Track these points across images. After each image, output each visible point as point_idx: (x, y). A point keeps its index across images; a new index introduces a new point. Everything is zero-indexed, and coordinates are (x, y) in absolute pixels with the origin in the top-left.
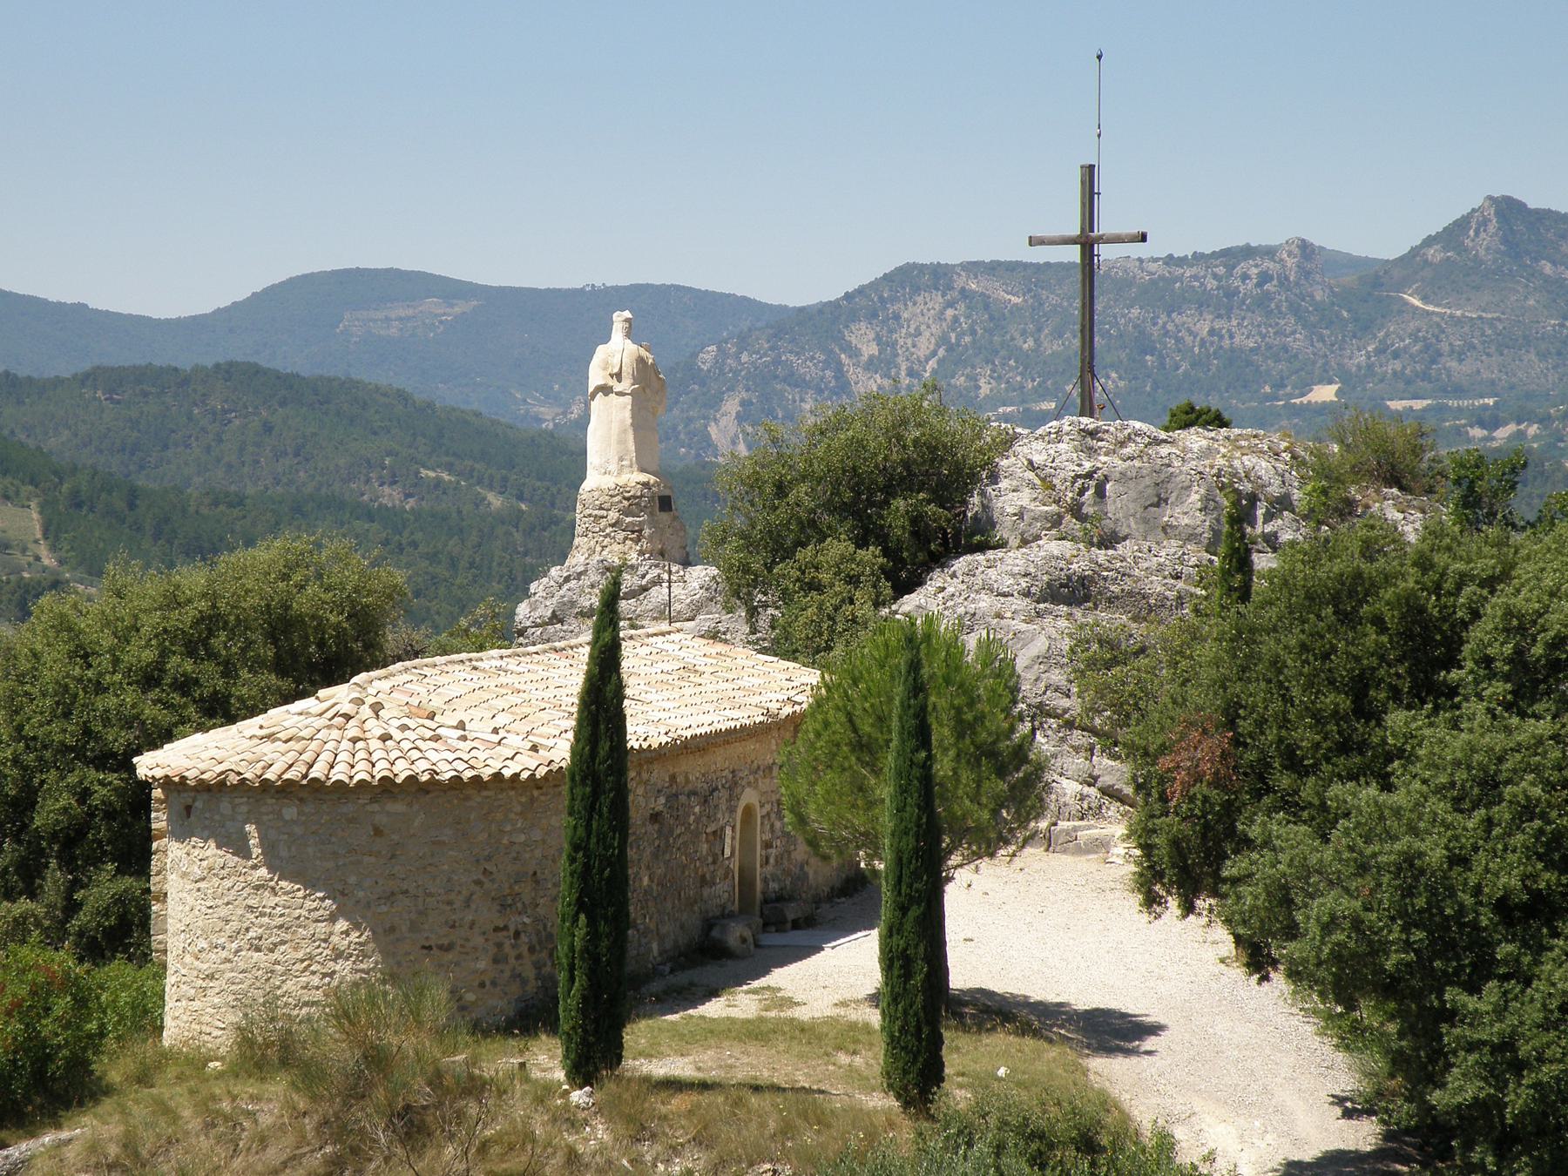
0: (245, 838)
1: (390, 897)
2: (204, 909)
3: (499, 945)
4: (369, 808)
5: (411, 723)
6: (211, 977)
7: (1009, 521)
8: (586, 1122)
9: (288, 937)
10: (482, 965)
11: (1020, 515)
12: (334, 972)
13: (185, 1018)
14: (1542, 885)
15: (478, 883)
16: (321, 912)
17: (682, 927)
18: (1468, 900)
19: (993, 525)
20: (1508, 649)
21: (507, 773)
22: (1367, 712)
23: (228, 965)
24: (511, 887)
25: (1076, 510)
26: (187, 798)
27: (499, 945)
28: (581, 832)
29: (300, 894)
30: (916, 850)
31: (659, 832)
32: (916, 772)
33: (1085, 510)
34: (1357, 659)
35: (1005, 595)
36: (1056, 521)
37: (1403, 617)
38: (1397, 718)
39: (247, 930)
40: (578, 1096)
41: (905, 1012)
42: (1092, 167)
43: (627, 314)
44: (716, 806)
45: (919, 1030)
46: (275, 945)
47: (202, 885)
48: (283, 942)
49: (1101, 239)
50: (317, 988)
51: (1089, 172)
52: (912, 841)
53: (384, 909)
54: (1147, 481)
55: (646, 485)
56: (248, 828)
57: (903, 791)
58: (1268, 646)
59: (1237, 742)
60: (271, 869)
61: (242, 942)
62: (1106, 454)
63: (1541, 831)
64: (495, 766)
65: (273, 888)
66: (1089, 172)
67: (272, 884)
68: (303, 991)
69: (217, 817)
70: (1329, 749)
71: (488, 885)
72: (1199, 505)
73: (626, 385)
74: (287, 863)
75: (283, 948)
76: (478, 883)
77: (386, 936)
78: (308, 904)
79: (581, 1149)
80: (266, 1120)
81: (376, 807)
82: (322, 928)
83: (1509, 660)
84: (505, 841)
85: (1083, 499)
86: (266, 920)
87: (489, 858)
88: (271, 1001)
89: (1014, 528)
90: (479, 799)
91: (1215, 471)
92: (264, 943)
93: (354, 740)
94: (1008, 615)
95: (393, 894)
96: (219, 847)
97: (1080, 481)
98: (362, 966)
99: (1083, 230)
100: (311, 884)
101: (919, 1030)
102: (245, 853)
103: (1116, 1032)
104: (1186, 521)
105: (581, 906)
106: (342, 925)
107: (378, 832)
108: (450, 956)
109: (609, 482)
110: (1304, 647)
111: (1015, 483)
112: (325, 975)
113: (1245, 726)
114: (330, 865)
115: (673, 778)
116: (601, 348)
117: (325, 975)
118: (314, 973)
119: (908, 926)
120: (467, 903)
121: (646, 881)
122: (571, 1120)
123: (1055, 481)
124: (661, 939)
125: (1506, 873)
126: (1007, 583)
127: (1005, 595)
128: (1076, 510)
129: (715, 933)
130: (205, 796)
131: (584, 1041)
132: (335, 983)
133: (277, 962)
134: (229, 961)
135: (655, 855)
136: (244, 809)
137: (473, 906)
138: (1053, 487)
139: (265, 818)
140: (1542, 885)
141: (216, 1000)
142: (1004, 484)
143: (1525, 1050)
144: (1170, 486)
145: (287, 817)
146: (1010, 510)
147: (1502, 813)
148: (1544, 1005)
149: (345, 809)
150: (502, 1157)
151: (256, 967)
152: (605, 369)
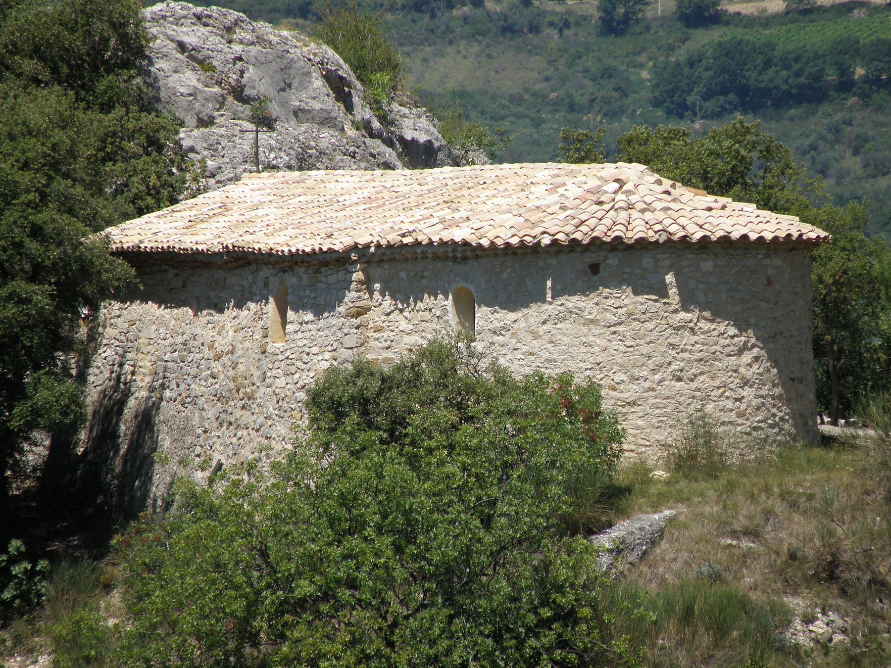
2: (623, 348)
6: (633, 404)
9: (706, 369)
12: (743, 397)
16: (732, 348)
25: (238, 92)
26: (590, 258)
29: (715, 333)
39: (669, 364)
46: (695, 376)
47: (620, 329)
48: (702, 373)
50: (731, 410)
54: (274, 66)
65: (692, 329)
67: (692, 325)
69: (638, 271)
75: (702, 378)
78: (722, 341)
81: (767, 261)
86: (686, 355)
91: (317, 59)
96: (636, 293)
97: (239, 64)
98: (762, 393)
102: (661, 292)
104: (317, 105)
107: (769, 283)
112: (736, 400)
117: (736, 400)
118: (728, 398)
123: (215, 63)
128: (238, 92)
132: (743, 407)
134: (653, 390)
136: (667, 263)
138: (212, 68)
139: (685, 270)
141: (640, 423)
144: (292, 71)
145: (704, 269)
151: (680, 393)
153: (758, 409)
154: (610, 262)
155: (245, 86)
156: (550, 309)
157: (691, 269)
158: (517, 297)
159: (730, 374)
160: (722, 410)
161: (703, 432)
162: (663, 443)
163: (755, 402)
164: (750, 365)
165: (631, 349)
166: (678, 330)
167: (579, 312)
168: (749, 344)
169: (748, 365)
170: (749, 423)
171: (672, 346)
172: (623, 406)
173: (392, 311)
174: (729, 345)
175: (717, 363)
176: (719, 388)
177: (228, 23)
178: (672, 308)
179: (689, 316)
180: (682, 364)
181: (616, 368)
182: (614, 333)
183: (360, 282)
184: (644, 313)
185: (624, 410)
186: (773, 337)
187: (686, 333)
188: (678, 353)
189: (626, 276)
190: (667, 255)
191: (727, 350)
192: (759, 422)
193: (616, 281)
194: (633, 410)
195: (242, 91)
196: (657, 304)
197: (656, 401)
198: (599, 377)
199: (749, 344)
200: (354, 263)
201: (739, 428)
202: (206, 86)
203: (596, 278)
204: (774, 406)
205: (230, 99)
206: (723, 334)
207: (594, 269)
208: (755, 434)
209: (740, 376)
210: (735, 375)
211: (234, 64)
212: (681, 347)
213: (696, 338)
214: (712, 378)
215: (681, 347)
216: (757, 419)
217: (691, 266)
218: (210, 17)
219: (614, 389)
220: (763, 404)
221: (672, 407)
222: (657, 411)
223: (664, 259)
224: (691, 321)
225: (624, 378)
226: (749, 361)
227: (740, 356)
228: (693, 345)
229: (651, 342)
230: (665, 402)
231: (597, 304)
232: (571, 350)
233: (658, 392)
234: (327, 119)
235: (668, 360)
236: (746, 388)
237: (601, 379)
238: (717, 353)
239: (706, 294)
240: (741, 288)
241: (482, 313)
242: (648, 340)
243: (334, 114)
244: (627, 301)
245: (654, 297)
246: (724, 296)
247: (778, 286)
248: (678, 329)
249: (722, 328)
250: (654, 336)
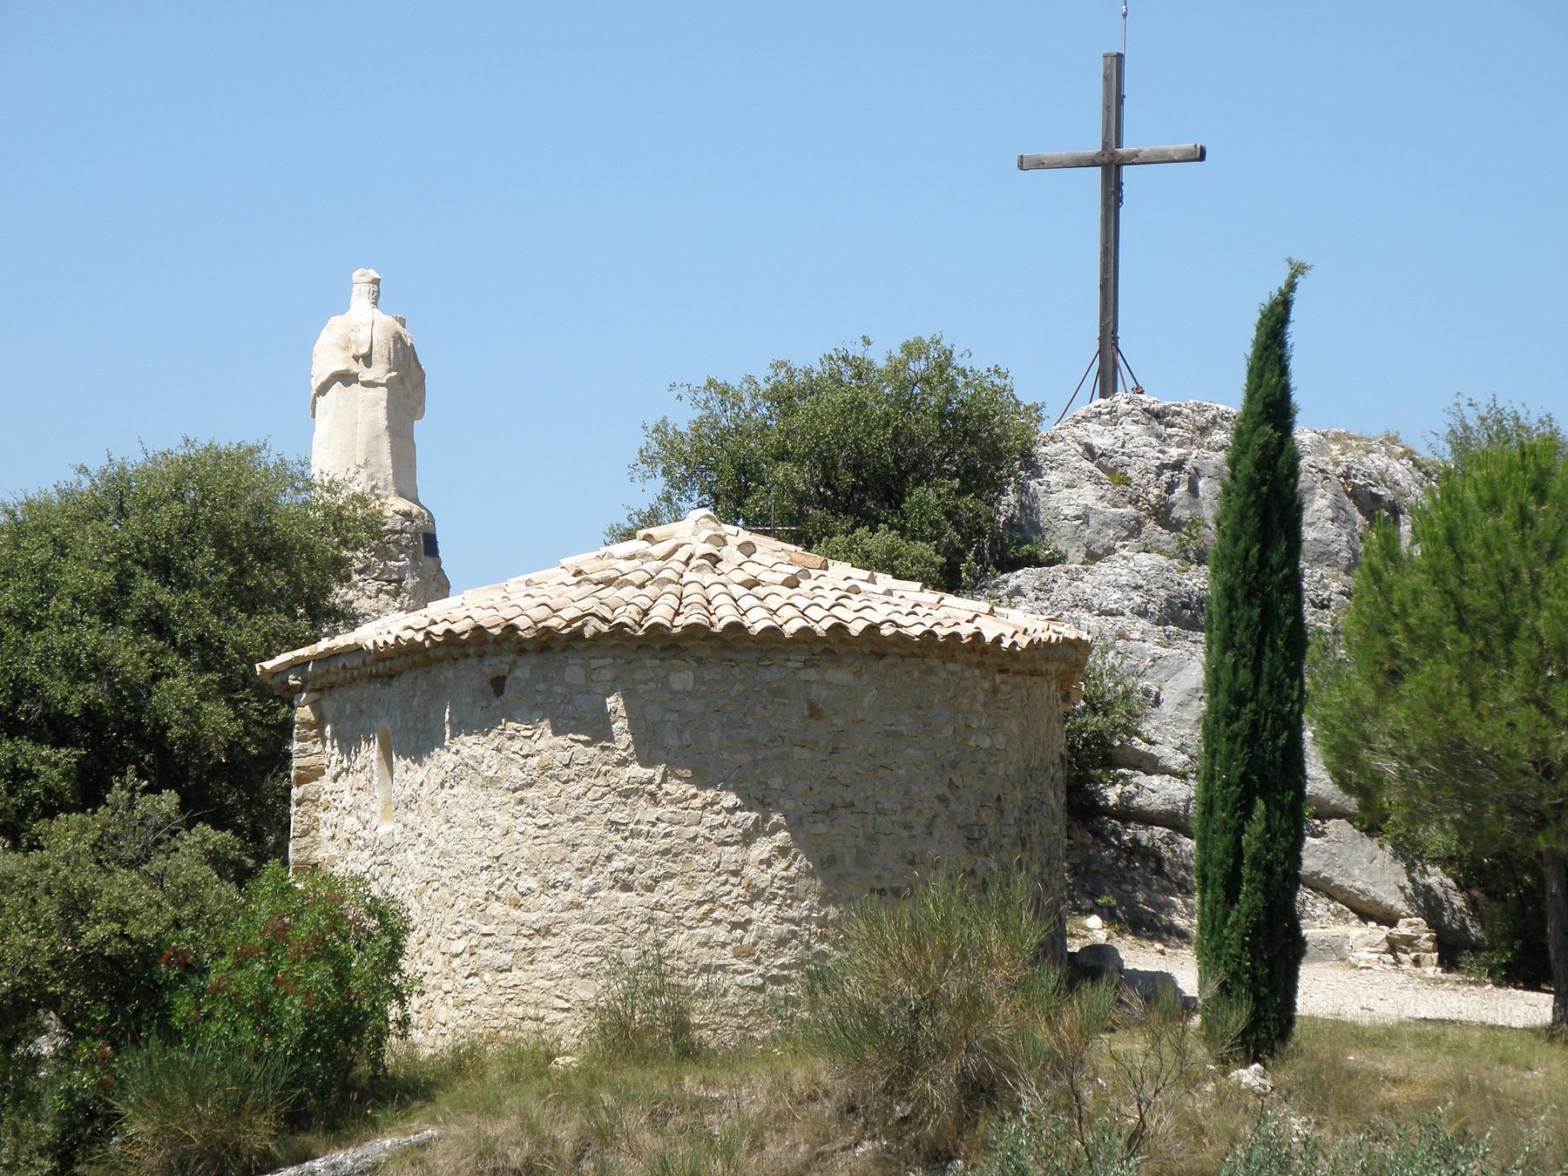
1: (829, 811)
2: (531, 830)
4: (803, 675)
6: (545, 932)
7: (1067, 527)
9: (677, 868)
11: (1084, 518)
12: (749, 921)
13: (489, 1000)
15: (943, 800)
16: (730, 830)
23: (576, 913)
24: (977, 814)
25: (1162, 514)
26: (492, 666)
28: (1244, 676)
29: (697, 803)
33: (1177, 513)
35: (1111, 613)
36: (1134, 529)
39: (609, 858)
42: (1120, 57)
43: (373, 274)
47: (529, 794)
48: (669, 876)
49: (1134, 159)
50: (724, 945)
51: (1116, 64)
53: (822, 828)
55: (407, 515)
61: (601, 876)
62: (1179, 446)
65: (652, 795)
66: (1116, 64)
67: (652, 787)
69: (558, 689)
72: (1329, 513)
73: (379, 371)
75: (668, 885)
78: (710, 818)
81: (812, 674)
82: (731, 854)
84: (972, 743)
85: (1173, 498)
87: (954, 765)
88: (657, 965)
89: (1076, 535)
90: (943, 674)
91: (1340, 470)
92: (639, 878)
94: (1137, 635)
95: (833, 807)
96: (556, 732)
97: (1168, 473)
98: (792, 913)
99: (1105, 145)
107: (815, 712)
111: (1068, 476)
112: (735, 926)
114: (744, 758)
116: (335, 320)
117: (735, 926)
118: (717, 922)
123: (1131, 473)
126: (1112, 598)
127: (1111, 613)
128: (1162, 514)
133: (660, 906)
134: (579, 906)
136: (607, 675)
137: (937, 834)
138: (1126, 481)
139: (641, 688)
141: (555, 967)
142: (1053, 477)
145: (676, 687)
146: (1070, 511)
149: (768, 677)
152: (346, 348)
153: (782, 942)
154: (518, 673)
155: (1173, 505)
156: (443, 759)
157: (652, 685)
158: (415, 741)
159: (723, 878)
160: (705, 944)
161: (654, 976)
162: (592, 1004)
163: (774, 930)
164: (768, 863)
165: (546, 832)
166: (627, 797)
167: (476, 765)
168: (768, 827)
169: (761, 862)
170: (761, 969)
171: (614, 825)
172: (530, 937)
173: (339, 774)
174: (722, 826)
175: (697, 857)
176: (700, 904)
177: (1201, 420)
178: (615, 757)
179: (650, 772)
180: (631, 859)
181: (521, 866)
182: (521, 802)
183: (305, 724)
184: (567, 766)
185: (531, 944)
186: (827, 812)
187: (642, 801)
188: (625, 839)
189: (539, 698)
190: (609, 660)
191: (723, 833)
192: (783, 967)
193: (530, 711)
194: (544, 943)
195: (1169, 512)
196: (592, 750)
197: (584, 926)
198: (498, 882)
199: (768, 827)
200: (300, 689)
201: (739, 979)
202: (1115, 506)
203: (496, 703)
204: (823, 938)
205: (1150, 524)
206: (712, 804)
207: (498, 685)
208: (770, 988)
209: (744, 883)
210: (733, 880)
211: (1158, 475)
212: (632, 826)
213: (660, 811)
214: (689, 886)
215: (632, 826)
216: (779, 962)
217: (651, 680)
218: (1179, 414)
219: (518, 906)
220: (794, 934)
221: (610, 938)
222: (585, 946)
223: (604, 667)
224: (651, 781)
225: (533, 883)
226: (766, 855)
227: (747, 845)
228: (654, 825)
229: (576, 819)
230: (598, 928)
231: (499, 750)
232: (466, 835)
233: (587, 910)
234: (1323, 553)
235: (606, 851)
236: (757, 904)
237: (500, 887)
238: (699, 840)
239: (680, 735)
240: (750, 721)
241: (400, 764)
242: (573, 814)
243: (1335, 547)
244: (541, 744)
245: (582, 737)
246: (714, 737)
247: (838, 721)
248: (626, 794)
249: (710, 794)
250: (582, 808)
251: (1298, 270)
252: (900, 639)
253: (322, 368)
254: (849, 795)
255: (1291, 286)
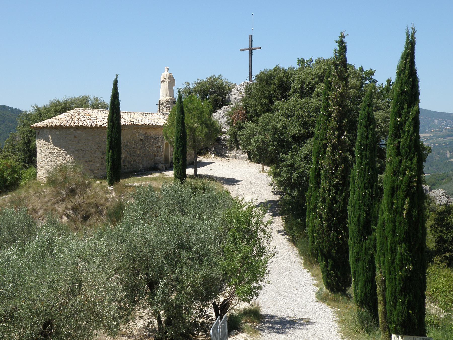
0: (48, 138)
1: (78, 150)
3: (102, 161)
5: (85, 117)
6: (43, 167)
8: (111, 193)
10: (98, 165)
11: (235, 99)
14: (302, 132)
15: (97, 148)
17: (149, 163)
18: (286, 135)
19: (230, 101)
20: (299, 86)
21: (103, 126)
22: (271, 102)
27: (102, 161)
30: (180, 136)
31: (142, 143)
32: (181, 120)
34: (270, 92)
37: (279, 82)
38: (277, 103)
40: (110, 188)
41: (178, 170)
44: (158, 141)
45: (181, 174)
51: (251, 36)
52: (180, 134)
55: (171, 99)
56: (49, 136)
57: (178, 124)
58: (253, 91)
59: (247, 112)
60: (54, 145)
63: (302, 121)
64: (101, 124)
66: (251, 36)
68: (63, 170)
70: (264, 111)
71: (99, 149)
73: (167, 80)
74: (57, 143)
76: (97, 148)
77: (77, 158)
78: (61, 152)
79: (108, 198)
80: (46, 193)
81: (75, 132)
83: (299, 89)
87: (100, 143)
93: (72, 119)
100: (62, 147)
101: (181, 174)
103: (232, 182)
105: (110, 148)
106: (68, 156)
107: (75, 137)
108: (91, 163)
109: (164, 99)
110: (259, 90)
113: (248, 108)
115: (146, 133)
119: (179, 152)
120: (95, 152)
121: (139, 152)
122: (108, 192)
124: (143, 165)
125: (295, 129)
129: (157, 166)
130: (41, 130)
131: (111, 177)
135: (141, 148)
140: (302, 132)
143: (296, 166)
147: (295, 118)
148: (301, 157)
150: (92, 199)
251: (117, 75)
252: (96, 126)
253: (162, 79)
254: (81, 148)
255: (117, 77)
